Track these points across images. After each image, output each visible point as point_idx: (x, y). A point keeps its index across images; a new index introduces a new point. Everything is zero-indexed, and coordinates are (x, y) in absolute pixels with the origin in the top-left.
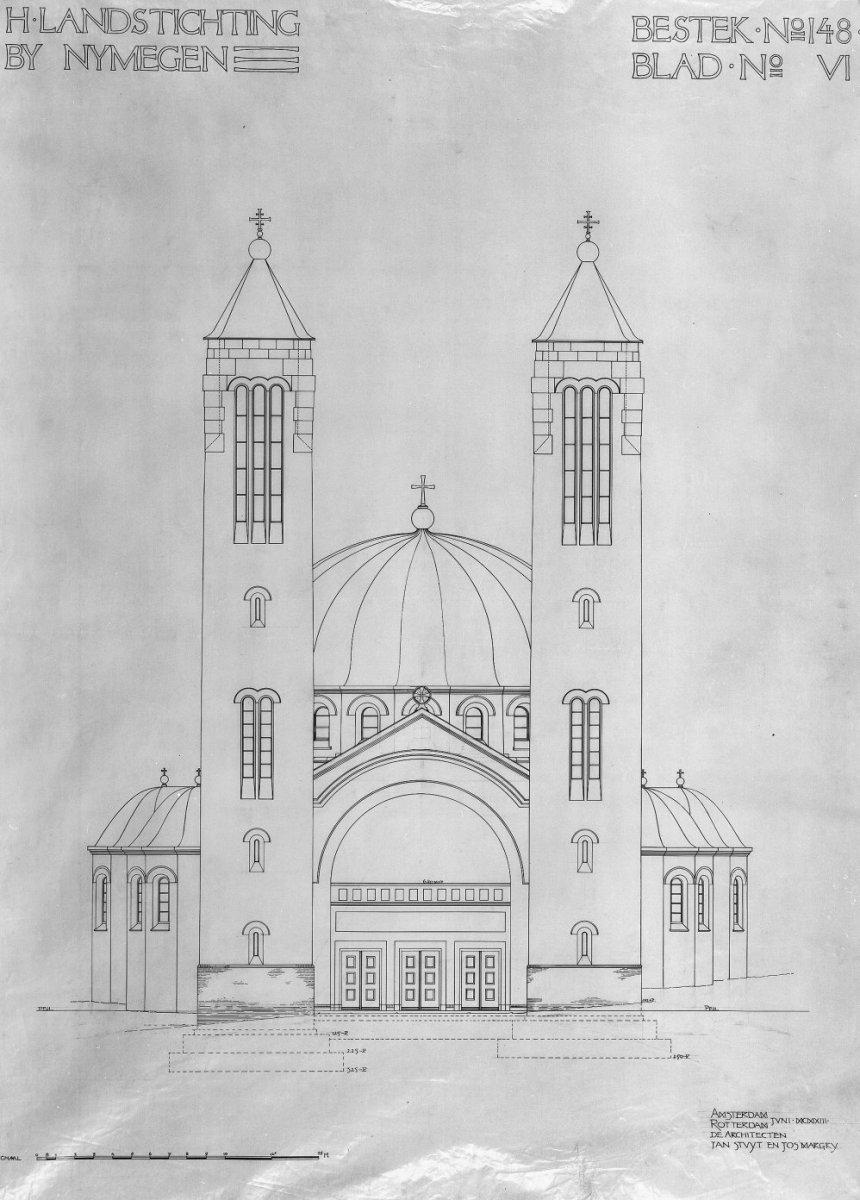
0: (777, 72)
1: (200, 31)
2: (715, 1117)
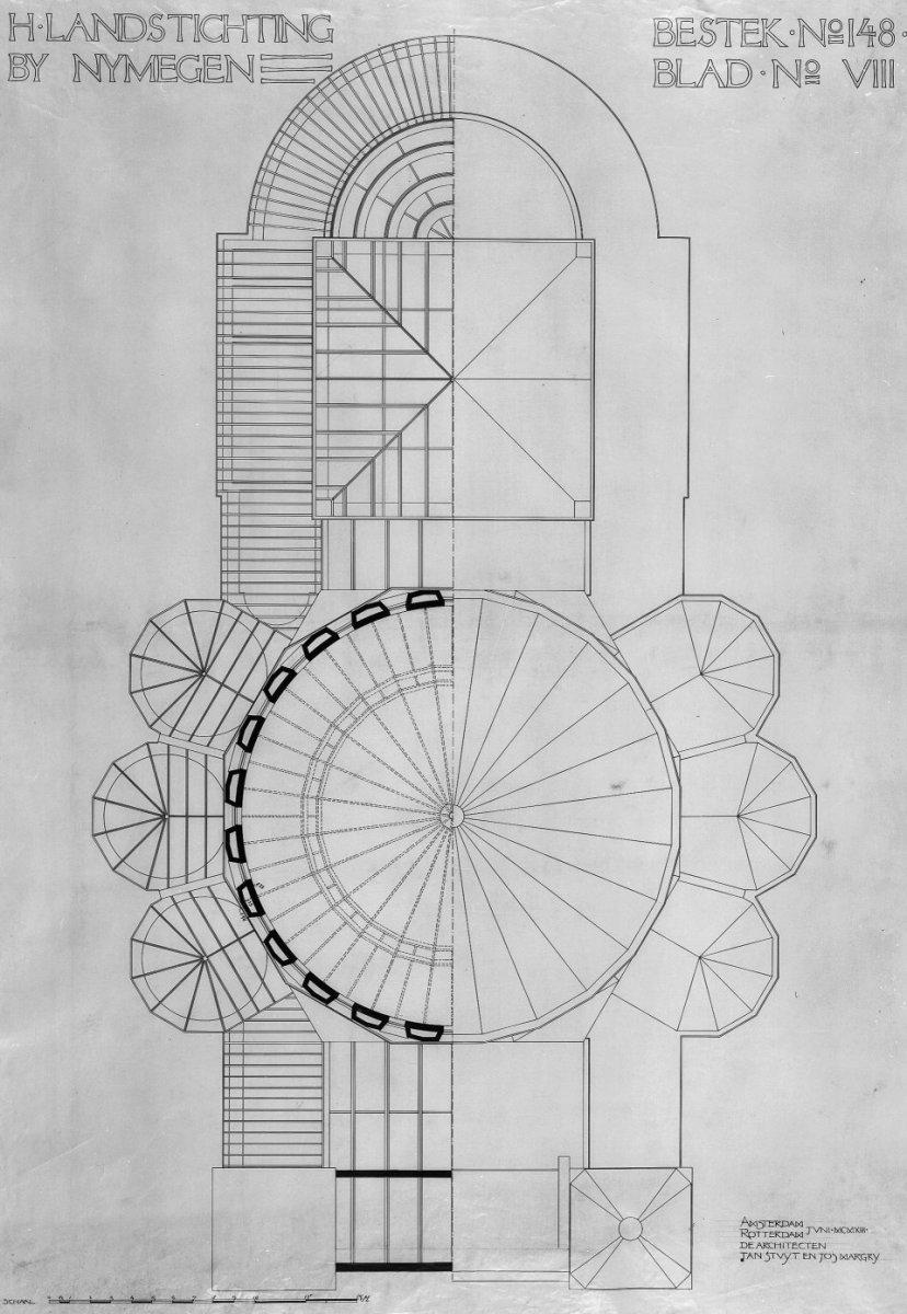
0: (813, 78)
1: (224, 38)
2: (745, 1226)
